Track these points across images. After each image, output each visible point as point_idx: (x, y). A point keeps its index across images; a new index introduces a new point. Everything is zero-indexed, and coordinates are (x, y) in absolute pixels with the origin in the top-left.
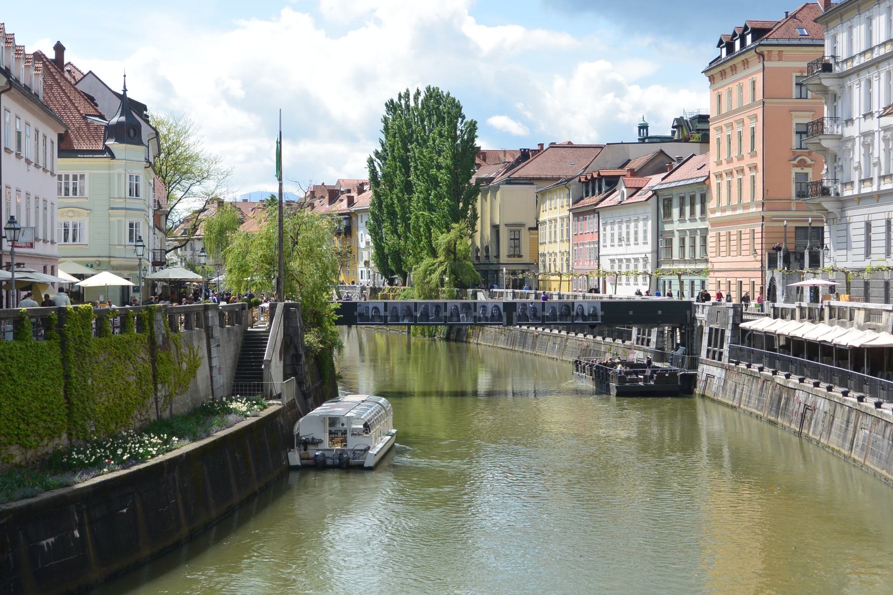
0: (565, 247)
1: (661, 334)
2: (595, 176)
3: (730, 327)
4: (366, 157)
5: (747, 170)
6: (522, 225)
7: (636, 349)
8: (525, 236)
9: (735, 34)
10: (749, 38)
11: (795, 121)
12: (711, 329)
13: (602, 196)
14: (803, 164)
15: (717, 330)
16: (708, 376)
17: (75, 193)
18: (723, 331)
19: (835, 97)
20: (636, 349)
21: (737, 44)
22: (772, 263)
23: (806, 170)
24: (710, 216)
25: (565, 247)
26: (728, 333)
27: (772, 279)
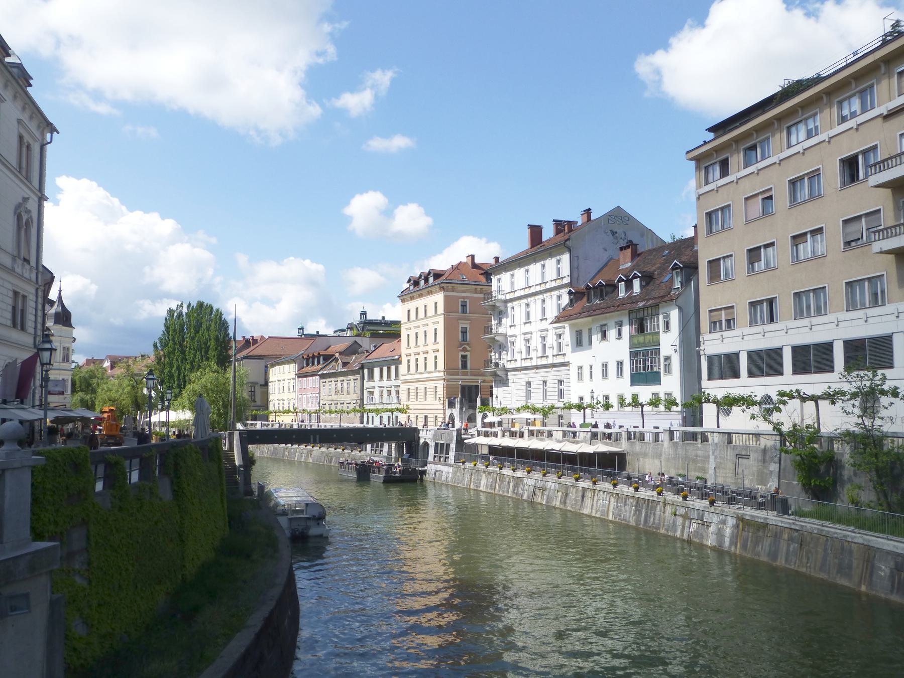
0: (292, 395)
1: (390, 448)
2: (316, 354)
3: (454, 442)
4: (152, 343)
5: (431, 352)
6: (256, 383)
7: (384, 454)
8: (258, 391)
9: (420, 276)
10: (637, 284)
11: (461, 326)
12: (436, 444)
13: (320, 366)
14: (465, 350)
15: (442, 445)
16: (436, 471)
17: (605, 366)
18: (448, 446)
19: (500, 313)
20: (384, 454)
21: (422, 283)
22: (451, 405)
23: (466, 353)
24: (401, 377)
25: (292, 395)
26: (453, 446)
27: (451, 415)
